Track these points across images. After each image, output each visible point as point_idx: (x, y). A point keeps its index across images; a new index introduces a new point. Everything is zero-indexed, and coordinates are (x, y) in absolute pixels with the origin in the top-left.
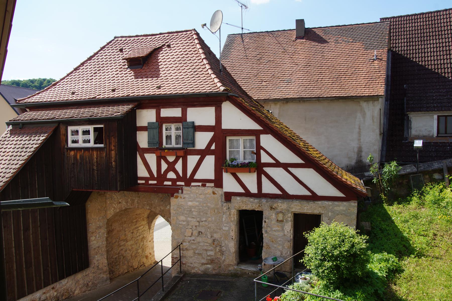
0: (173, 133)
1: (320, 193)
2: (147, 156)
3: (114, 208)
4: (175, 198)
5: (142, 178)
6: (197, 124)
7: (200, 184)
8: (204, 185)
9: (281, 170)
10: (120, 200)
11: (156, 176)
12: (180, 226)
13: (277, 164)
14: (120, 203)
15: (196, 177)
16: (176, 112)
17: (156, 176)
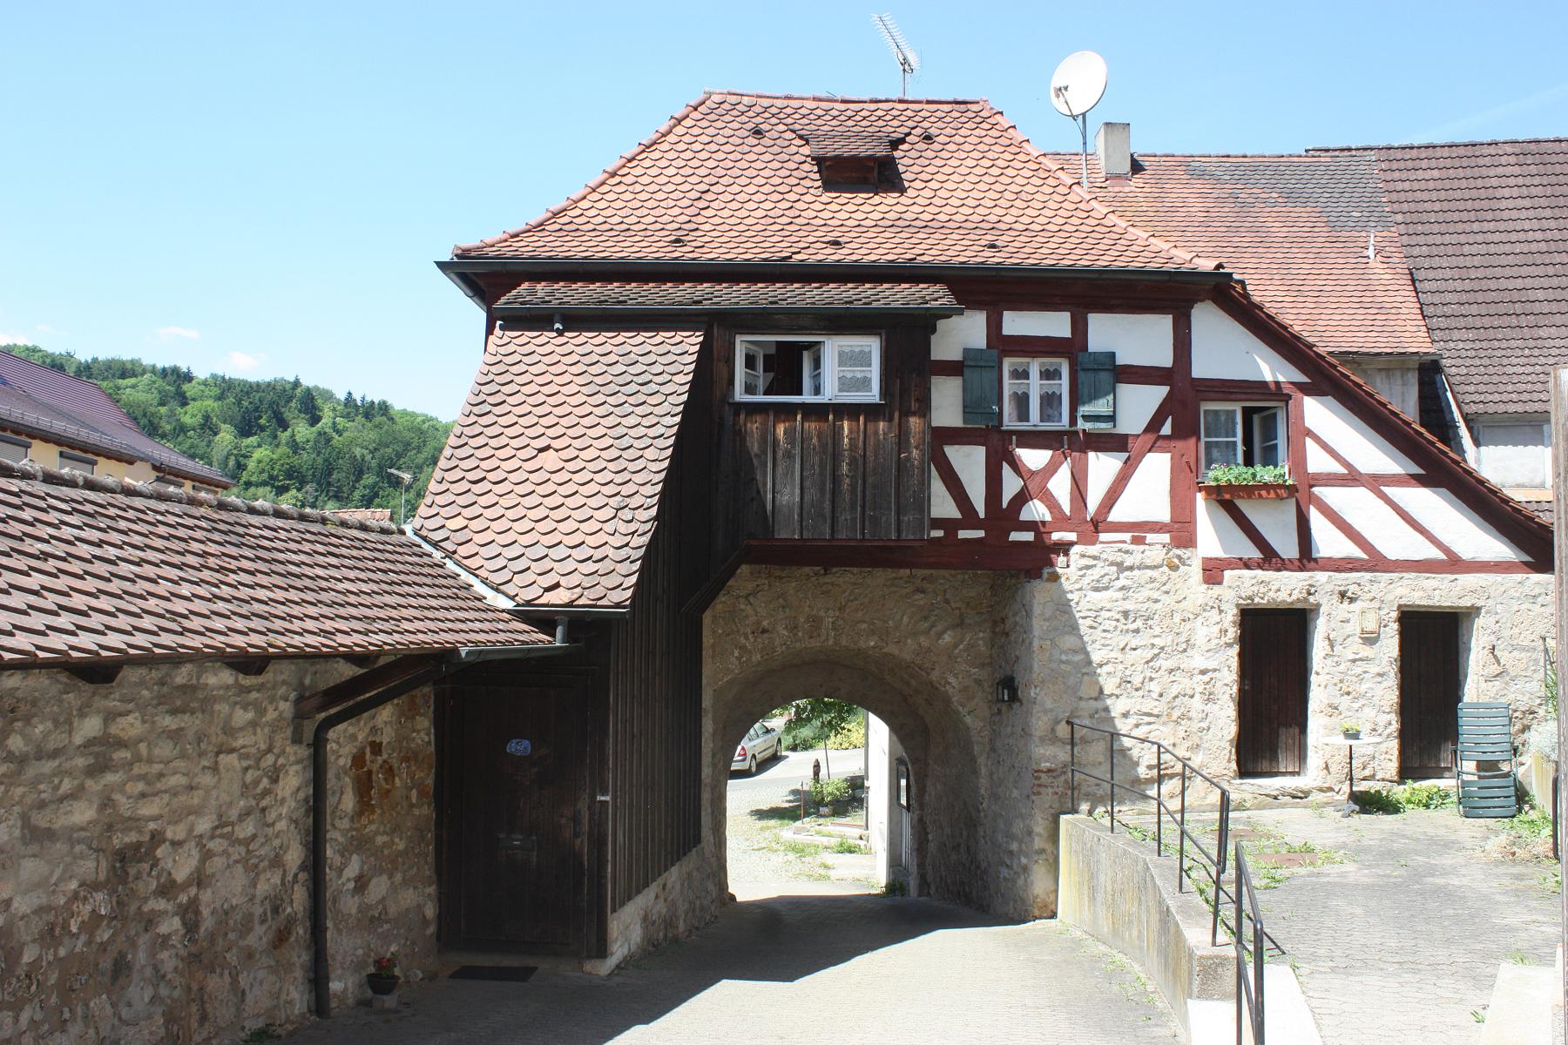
0: (1035, 387)
1: (1466, 554)
2: (955, 454)
3: (742, 648)
4: (1048, 580)
5: (938, 523)
6: (1121, 360)
7: (1127, 536)
8: (1138, 541)
9: (1361, 493)
10: (765, 623)
11: (982, 515)
12: (1063, 666)
13: (1352, 478)
14: (764, 631)
15: (1116, 515)
16: (1056, 324)
17: (982, 515)
